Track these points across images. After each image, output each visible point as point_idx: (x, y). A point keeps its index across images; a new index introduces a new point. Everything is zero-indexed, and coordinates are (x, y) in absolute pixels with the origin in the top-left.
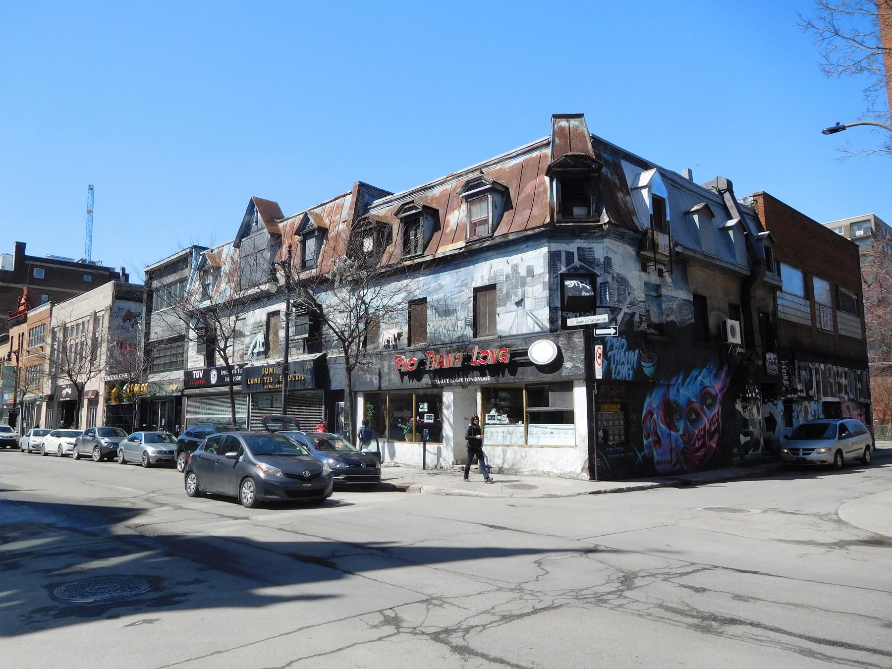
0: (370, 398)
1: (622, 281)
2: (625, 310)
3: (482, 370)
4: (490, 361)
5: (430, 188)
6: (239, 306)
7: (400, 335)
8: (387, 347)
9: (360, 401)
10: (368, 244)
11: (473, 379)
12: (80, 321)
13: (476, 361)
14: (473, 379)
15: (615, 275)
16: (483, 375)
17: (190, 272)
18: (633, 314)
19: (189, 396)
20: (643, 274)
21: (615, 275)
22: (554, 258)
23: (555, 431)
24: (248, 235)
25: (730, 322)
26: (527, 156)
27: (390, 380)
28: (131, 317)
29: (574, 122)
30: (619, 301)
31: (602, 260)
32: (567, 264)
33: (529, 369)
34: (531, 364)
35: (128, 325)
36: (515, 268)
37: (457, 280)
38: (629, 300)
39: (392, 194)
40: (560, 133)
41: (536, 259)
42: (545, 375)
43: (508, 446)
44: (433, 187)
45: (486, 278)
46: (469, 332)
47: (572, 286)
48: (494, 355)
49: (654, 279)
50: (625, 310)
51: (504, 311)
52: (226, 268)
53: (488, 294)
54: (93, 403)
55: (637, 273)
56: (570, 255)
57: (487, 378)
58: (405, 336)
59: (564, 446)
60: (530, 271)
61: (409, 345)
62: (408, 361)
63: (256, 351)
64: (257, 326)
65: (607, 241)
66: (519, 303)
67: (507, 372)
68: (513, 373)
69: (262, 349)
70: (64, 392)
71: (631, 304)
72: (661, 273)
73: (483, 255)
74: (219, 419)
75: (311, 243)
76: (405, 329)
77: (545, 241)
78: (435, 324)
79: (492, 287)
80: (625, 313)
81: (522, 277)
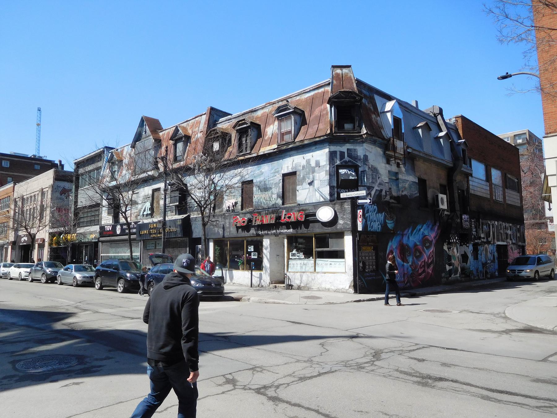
1: (375, 170)
2: (376, 188)
3: (288, 225)
4: (293, 219)
5: (255, 111)
6: (134, 185)
7: (236, 203)
8: (228, 211)
9: (211, 245)
10: (216, 146)
11: (282, 231)
12: (33, 195)
13: (284, 219)
14: (282, 231)
15: (370, 166)
16: (288, 228)
17: (103, 163)
18: (381, 190)
19: (102, 242)
20: (387, 166)
21: (370, 166)
22: (332, 155)
25: (441, 196)
26: (316, 92)
27: (230, 232)
28: (65, 192)
29: (345, 71)
30: (373, 182)
31: (362, 157)
33: (317, 225)
34: (318, 221)
35: (63, 196)
36: (308, 162)
37: (272, 169)
38: (378, 181)
39: (231, 115)
40: (336, 77)
41: (321, 156)
43: (304, 272)
45: (290, 167)
46: (280, 201)
47: (343, 173)
48: (295, 216)
49: (394, 168)
50: (376, 188)
52: (126, 161)
54: (41, 246)
55: (384, 165)
56: (342, 154)
57: (291, 230)
58: (239, 204)
59: (338, 273)
60: (318, 164)
61: (242, 209)
62: (241, 220)
63: (145, 213)
64: (146, 197)
65: (365, 145)
66: (311, 184)
68: (307, 227)
69: (149, 212)
70: (23, 239)
71: (380, 184)
72: (398, 165)
73: (288, 153)
75: (180, 145)
76: (240, 199)
77: (327, 144)
78: (258, 197)
79: (294, 174)
80: (376, 190)
81: (312, 167)
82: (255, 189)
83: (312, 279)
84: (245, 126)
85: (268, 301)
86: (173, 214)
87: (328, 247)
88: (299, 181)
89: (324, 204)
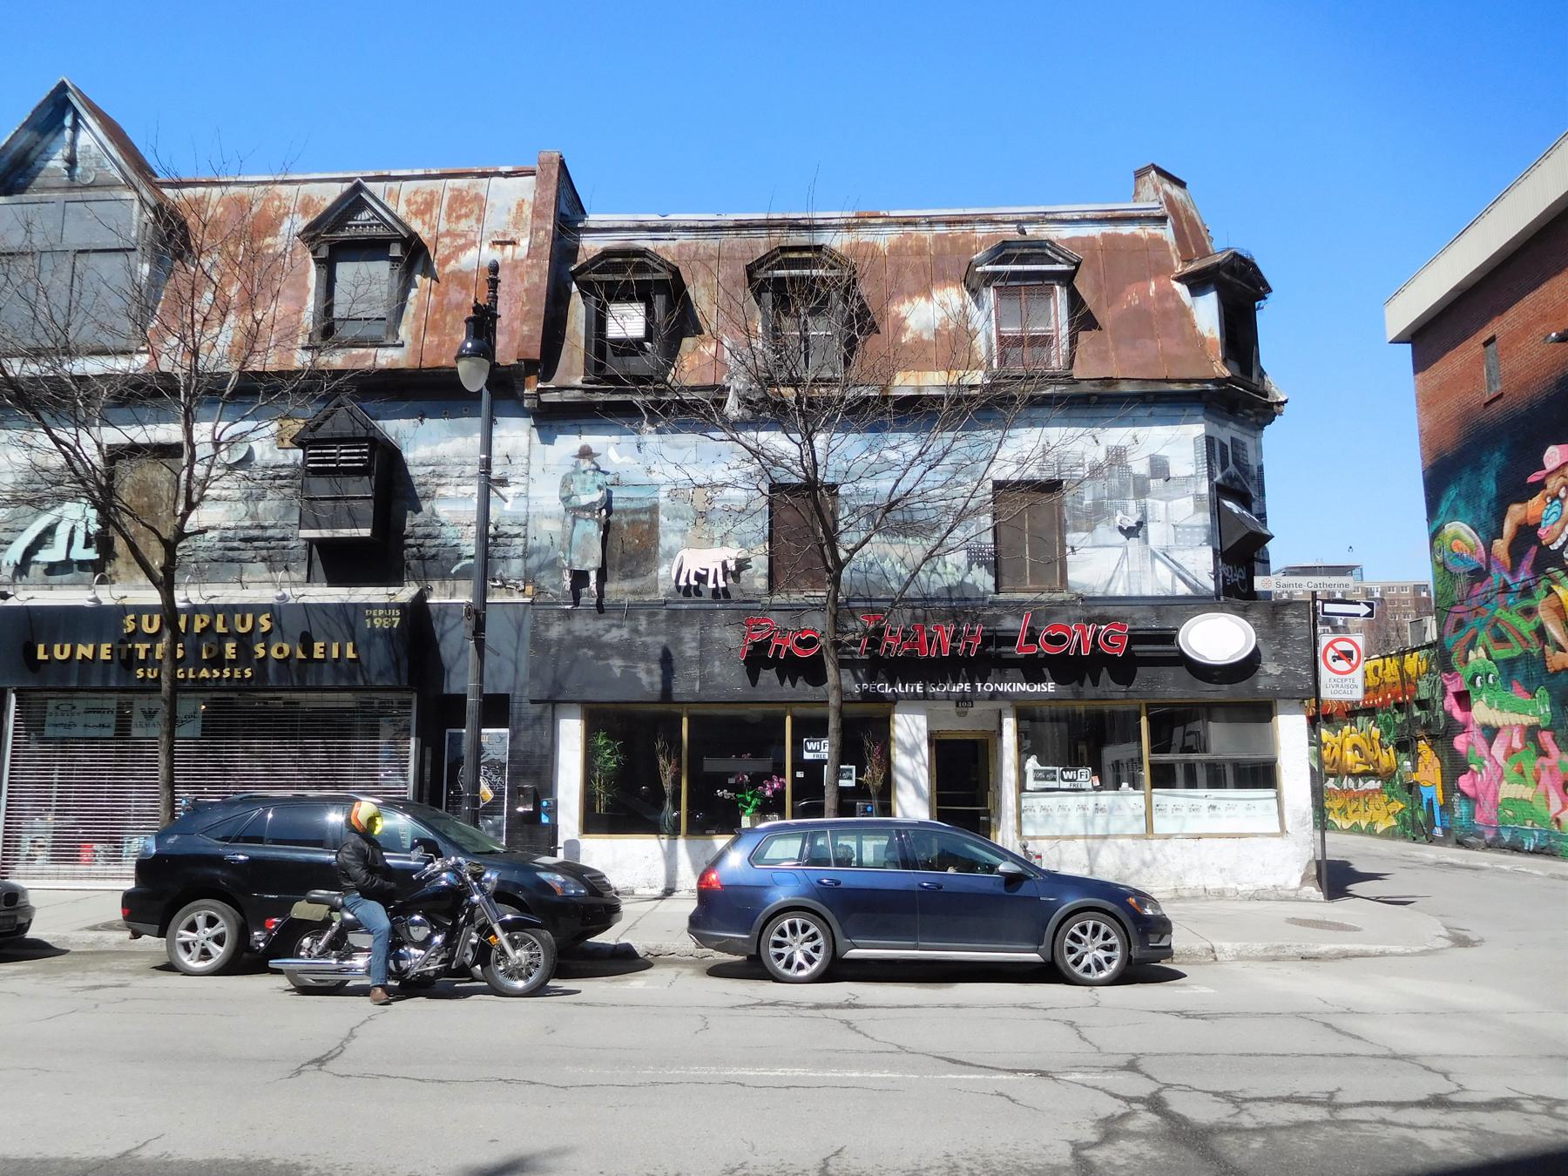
0: (598, 720)
7: (742, 565)
9: (571, 733)
16: (1034, 677)
23: (1222, 805)
24: (22, 189)
26: (1109, 229)
32: (1222, 470)
33: (1169, 673)
34: (1182, 660)
42: (1213, 687)
43: (1105, 837)
44: (819, 227)
51: (1089, 542)
57: (1049, 687)
58: (759, 564)
59: (1255, 835)
60: (1159, 468)
66: (1134, 531)
73: (1122, 411)
81: (1136, 477)
83: (1144, 863)
85: (1314, 950)
86: (295, 576)
88: (1075, 517)
89: (1197, 603)
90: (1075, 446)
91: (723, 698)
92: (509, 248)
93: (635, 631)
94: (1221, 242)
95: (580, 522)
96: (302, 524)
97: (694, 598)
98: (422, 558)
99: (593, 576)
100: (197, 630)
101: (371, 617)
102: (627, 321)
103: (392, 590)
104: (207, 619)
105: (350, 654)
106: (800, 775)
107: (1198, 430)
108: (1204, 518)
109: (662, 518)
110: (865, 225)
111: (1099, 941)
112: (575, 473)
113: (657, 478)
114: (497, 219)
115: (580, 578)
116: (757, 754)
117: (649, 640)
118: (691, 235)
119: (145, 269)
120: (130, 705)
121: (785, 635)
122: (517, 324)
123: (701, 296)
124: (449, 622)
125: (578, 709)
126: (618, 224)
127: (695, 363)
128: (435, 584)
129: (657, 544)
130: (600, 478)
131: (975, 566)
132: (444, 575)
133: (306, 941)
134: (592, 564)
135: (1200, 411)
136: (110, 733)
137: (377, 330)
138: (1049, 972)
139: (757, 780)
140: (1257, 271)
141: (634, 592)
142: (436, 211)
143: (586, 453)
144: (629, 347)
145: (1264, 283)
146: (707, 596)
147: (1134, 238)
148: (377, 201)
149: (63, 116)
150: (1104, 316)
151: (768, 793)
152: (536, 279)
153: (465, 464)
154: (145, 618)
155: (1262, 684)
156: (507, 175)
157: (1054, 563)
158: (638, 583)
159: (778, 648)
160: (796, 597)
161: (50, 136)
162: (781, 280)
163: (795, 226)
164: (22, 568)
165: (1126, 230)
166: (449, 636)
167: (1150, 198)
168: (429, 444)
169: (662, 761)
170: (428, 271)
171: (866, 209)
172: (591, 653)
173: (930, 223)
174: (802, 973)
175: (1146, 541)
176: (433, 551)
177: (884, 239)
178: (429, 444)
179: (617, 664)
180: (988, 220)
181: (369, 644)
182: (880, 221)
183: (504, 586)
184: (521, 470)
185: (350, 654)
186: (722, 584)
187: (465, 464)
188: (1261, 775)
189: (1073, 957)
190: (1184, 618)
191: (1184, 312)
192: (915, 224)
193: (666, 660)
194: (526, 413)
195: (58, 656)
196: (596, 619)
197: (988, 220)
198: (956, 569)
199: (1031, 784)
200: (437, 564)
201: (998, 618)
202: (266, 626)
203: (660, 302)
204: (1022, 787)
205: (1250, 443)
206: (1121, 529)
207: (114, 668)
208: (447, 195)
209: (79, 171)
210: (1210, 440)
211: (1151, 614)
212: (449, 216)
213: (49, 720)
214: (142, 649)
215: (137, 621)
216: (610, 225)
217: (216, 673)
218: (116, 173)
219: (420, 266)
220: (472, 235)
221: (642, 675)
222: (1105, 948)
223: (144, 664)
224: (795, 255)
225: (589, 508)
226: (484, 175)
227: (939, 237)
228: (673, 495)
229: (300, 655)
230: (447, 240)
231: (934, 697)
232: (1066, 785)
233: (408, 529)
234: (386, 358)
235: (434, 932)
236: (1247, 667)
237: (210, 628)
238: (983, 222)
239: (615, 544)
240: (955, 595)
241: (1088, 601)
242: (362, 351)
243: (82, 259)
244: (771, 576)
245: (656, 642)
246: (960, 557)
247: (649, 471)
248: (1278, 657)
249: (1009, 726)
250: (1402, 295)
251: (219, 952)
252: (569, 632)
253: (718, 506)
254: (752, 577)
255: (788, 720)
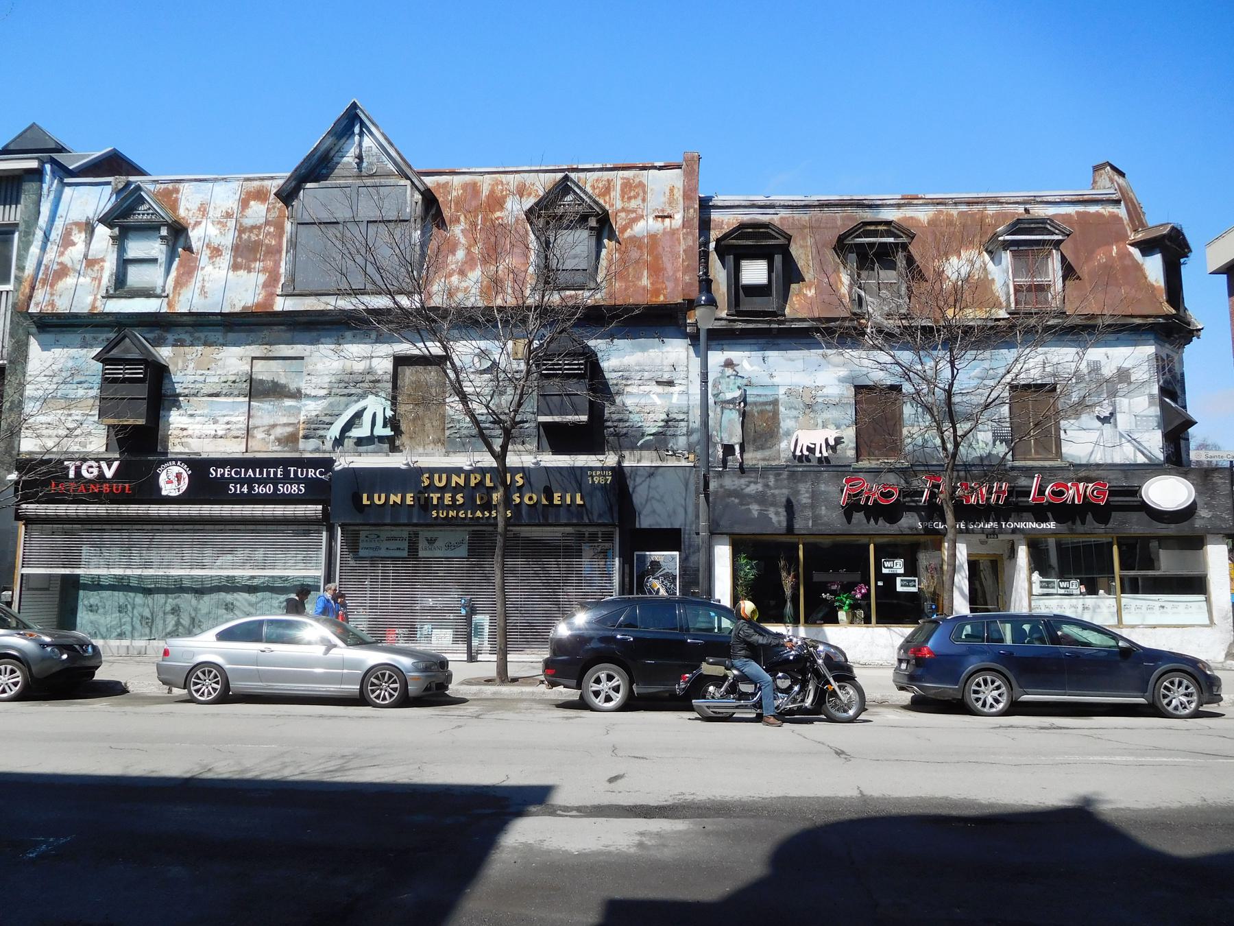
5: (870, 206)
7: (838, 441)
9: (723, 555)
11: (1021, 525)
14: (1021, 525)
16: (1041, 519)
19: (30, 521)
24: (325, 177)
26: (1081, 208)
27: (816, 518)
33: (1134, 516)
42: (1163, 525)
44: (878, 206)
53: (1041, 396)
57: (1052, 525)
63: (362, 431)
67: (1089, 517)
74: (181, 578)
82: (908, 410)
84: (891, 240)
87: (1153, 569)
89: (1152, 469)
90: (1058, 359)
91: (828, 532)
92: (667, 220)
93: (767, 486)
94: (1157, 219)
95: (726, 411)
96: (540, 412)
97: (805, 463)
98: (617, 435)
99: (737, 448)
100: (472, 484)
101: (592, 476)
102: (755, 272)
103: (601, 457)
104: (479, 478)
105: (579, 501)
106: (880, 584)
107: (1149, 350)
108: (1156, 410)
109: (782, 409)
110: (909, 204)
111: (1182, 690)
112: (722, 377)
113: (776, 380)
114: (656, 200)
115: (729, 449)
116: (850, 570)
117: (776, 492)
118: (789, 211)
119: (417, 234)
120: (416, 534)
121: (872, 490)
122: (680, 274)
123: (801, 253)
124: (638, 480)
125: (727, 539)
126: (737, 203)
127: (802, 303)
128: (627, 453)
129: (778, 426)
130: (739, 382)
131: (998, 443)
132: (633, 447)
133: (711, 689)
134: (736, 440)
135: (1152, 337)
136: (405, 554)
137: (579, 278)
138: (1153, 710)
139: (848, 588)
140: (1184, 238)
141: (764, 460)
142: (613, 194)
143: (729, 364)
144: (755, 291)
145: (1187, 246)
146: (814, 462)
147: (1098, 215)
148: (579, 188)
149: (353, 126)
150: (1084, 270)
151: (858, 596)
152: (691, 243)
153: (644, 370)
154: (436, 476)
155: (1198, 524)
156: (661, 168)
157: (1051, 441)
158: (767, 453)
159: (868, 498)
160: (874, 464)
161: (343, 141)
162: (862, 245)
163: (860, 205)
164: (339, 442)
165: (1092, 209)
166: (638, 489)
167: (1106, 186)
168: (619, 357)
169: (784, 574)
170: (612, 236)
171: (910, 192)
172: (737, 501)
173: (956, 203)
174: (994, 710)
175: (1116, 426)
176: (625, 430)
177: (923, 215)
178: (619, 357)
179: (755, 508)
180: (996, 202)
181: (591, 495)
182: (921, 201)
183: (674, 454)
184: (683, 375)
185: (579, 501)
186: (825, 454)
187: (644, 370)
188: (1195, 585)
189: (1166, 701)
190: (1145, 479)
191: (1138, 268)
192: (945, 204)
193: (789, 507)
194: (685, 335)
195: (377, 502)
196: (740, 477)
197: (996, 202)
198: (983, 442)
199: (1037, 589)
200: (627, 439)
201: (1016, 478)
202: (521, 482)
203: (778, 259)
204: (1031, 594)
205: (1176, 358)
206: (1098, 418)
207: (415, 510)
208: (619, 182)
209: (365, 165)
210: (1157, 357)
211: (1120, 475)
212: (623, 197)
213: (361, 545)
214: (435, 497)
215: (431, 478)
216: (732, 203)
217: (487, 514)
218: (391, 167)
219: (606, 233)
220: (640, 211)
221: (772, 516)
222: (1186, 695)
223: (436, 507)
224: (872, 228)
225: (732, 401)
226: (644, 168)
227: (961, 214)
228: (789, 393)
229: (544, 502)
230: (623, 215)
231: (973, 531)
232: (1062, 591)
233: (607, 415)
234: (587, 298)
235: (794, 683)
236: (1187, 513)
237: (481, 484)
238: (992, 203)
239: (750, 427)
240: (986, 462)
241: (1078, 466)
242: (573, 292)
243: (372, 227)
244: (857, 448)
245: (782, 493)
246: (989, 436)
247: (771, 376)
248: (1209, 506)
249: (1023, 553)
250: (1222, 240)
251: (618, 698)
252: (722, 486)
253: (820, 400)
254: (845, 450)
255: (872, 547)
